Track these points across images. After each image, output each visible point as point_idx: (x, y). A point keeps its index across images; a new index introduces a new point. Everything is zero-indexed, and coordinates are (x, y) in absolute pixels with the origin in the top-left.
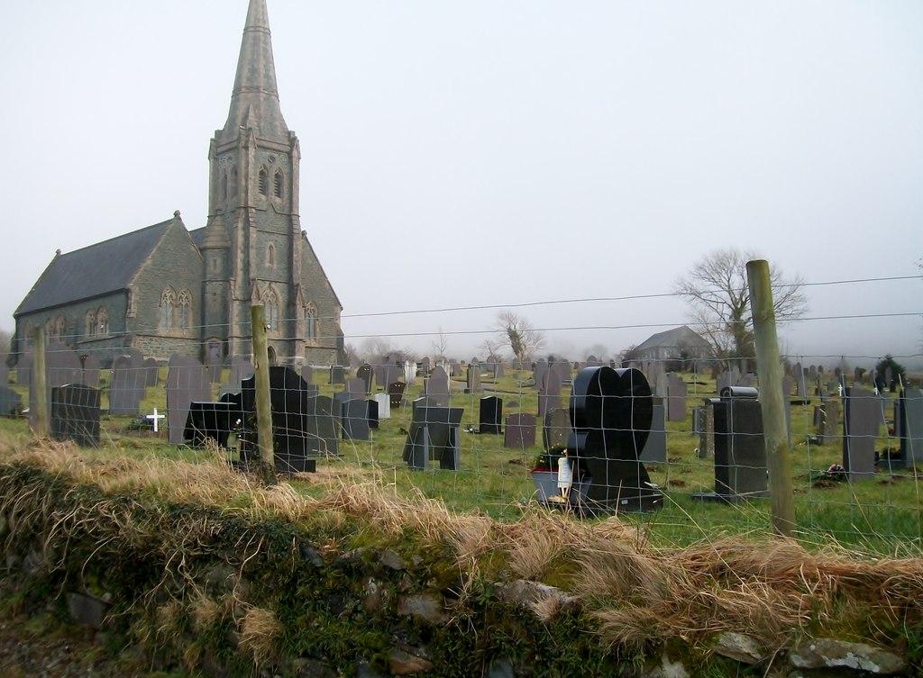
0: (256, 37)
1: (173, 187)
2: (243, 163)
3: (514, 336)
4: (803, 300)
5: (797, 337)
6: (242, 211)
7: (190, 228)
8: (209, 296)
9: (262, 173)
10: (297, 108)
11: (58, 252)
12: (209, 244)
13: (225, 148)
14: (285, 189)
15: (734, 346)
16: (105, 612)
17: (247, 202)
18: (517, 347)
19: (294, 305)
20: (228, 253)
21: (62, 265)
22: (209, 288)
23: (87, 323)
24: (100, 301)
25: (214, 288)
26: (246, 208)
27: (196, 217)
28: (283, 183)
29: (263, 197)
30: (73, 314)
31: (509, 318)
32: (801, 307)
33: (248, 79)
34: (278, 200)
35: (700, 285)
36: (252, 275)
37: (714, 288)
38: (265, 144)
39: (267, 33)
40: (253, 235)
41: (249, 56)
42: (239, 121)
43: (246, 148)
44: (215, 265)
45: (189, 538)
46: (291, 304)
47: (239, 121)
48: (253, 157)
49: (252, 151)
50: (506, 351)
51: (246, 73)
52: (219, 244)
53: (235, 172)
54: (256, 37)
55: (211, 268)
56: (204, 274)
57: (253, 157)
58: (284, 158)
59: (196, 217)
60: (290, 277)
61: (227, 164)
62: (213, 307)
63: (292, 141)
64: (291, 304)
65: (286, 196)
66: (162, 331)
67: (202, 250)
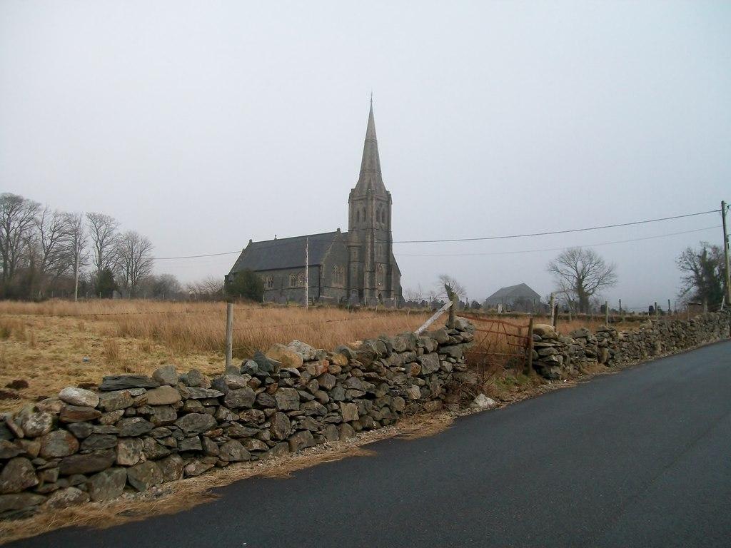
2: (370, 206)
3: (448, 288)
4: (615, 276)
5: (253, 242)
8: (352, 269)
10: (389, 180)
11: (251, 241)
13: (355, 197)
14: (386, 218)
15: (578, 299)
16: (291, 421)
18: (451, 295)
19: (391, 274)
20: (362, 250)
21: (253, 251)
22: (352, 265)
23: (290, 280)
28: (385, 216)
30: (280, 274)
31: (445, 278)
32: (613, 279)
35: (561, 267)
36: (375, 260)
37: (569, 269)
38: (380, 198)
40: (375, 240)
43: (372, 200)
44: (355, 255)
45: (535, 385)
47: (366, 186)
49: (374, 202)
50: (444, 297)
51: (368, 162)
53: (365, 211)
55: (353, 255)
56: (350, 258)
57: (370, 201)
59: (345, 229)
61: (360, 206)
62: (354, 274)
63: (389, 196)
65: (386, 222)
66: (334, 285)
67: (349, 247)
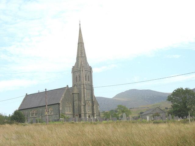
0: (81, 44)
1: (66, 81)
6: (83, 85)
7: (98, 93)
9: (85, 76)
10: (91, 61)
11: (26, 94)
12: (74, 93)
14: (90, 80)
17: (83, 83)
20: (79, 94)
22: (75, 102)
24: (50, 106)
25: (76, 103)
26: (83, 84)
27: (71, 86)
28: (89, 77)
29: (86, 82)
33: (81, 55)
34: (89, 82)
39: (83, 43)
41: (80, 49)
42: (80, 64)
44: (76, 97)
46: (93, 106)
48: (82, 71)
52: (77, 92)
54: (81, 44)
55: (75, 98)
57: (82, 71)
58: (89, 72)
59: (71, 86)
60: (92, 100)
61: (77, 74)
64: (93, 106)
